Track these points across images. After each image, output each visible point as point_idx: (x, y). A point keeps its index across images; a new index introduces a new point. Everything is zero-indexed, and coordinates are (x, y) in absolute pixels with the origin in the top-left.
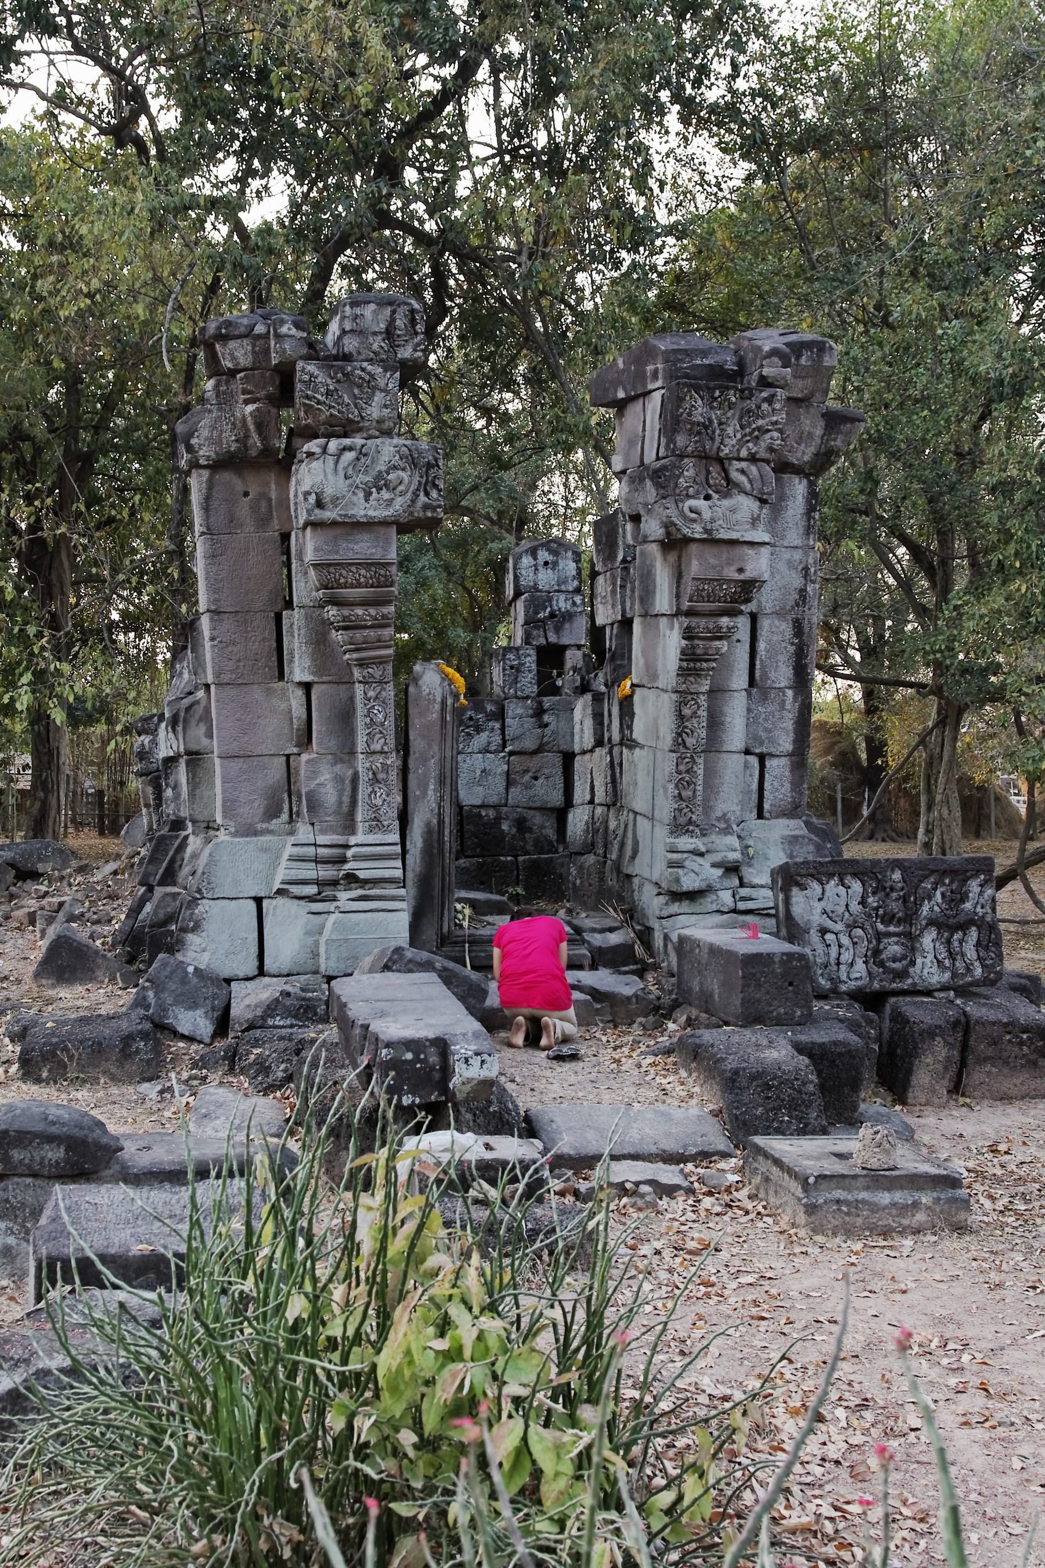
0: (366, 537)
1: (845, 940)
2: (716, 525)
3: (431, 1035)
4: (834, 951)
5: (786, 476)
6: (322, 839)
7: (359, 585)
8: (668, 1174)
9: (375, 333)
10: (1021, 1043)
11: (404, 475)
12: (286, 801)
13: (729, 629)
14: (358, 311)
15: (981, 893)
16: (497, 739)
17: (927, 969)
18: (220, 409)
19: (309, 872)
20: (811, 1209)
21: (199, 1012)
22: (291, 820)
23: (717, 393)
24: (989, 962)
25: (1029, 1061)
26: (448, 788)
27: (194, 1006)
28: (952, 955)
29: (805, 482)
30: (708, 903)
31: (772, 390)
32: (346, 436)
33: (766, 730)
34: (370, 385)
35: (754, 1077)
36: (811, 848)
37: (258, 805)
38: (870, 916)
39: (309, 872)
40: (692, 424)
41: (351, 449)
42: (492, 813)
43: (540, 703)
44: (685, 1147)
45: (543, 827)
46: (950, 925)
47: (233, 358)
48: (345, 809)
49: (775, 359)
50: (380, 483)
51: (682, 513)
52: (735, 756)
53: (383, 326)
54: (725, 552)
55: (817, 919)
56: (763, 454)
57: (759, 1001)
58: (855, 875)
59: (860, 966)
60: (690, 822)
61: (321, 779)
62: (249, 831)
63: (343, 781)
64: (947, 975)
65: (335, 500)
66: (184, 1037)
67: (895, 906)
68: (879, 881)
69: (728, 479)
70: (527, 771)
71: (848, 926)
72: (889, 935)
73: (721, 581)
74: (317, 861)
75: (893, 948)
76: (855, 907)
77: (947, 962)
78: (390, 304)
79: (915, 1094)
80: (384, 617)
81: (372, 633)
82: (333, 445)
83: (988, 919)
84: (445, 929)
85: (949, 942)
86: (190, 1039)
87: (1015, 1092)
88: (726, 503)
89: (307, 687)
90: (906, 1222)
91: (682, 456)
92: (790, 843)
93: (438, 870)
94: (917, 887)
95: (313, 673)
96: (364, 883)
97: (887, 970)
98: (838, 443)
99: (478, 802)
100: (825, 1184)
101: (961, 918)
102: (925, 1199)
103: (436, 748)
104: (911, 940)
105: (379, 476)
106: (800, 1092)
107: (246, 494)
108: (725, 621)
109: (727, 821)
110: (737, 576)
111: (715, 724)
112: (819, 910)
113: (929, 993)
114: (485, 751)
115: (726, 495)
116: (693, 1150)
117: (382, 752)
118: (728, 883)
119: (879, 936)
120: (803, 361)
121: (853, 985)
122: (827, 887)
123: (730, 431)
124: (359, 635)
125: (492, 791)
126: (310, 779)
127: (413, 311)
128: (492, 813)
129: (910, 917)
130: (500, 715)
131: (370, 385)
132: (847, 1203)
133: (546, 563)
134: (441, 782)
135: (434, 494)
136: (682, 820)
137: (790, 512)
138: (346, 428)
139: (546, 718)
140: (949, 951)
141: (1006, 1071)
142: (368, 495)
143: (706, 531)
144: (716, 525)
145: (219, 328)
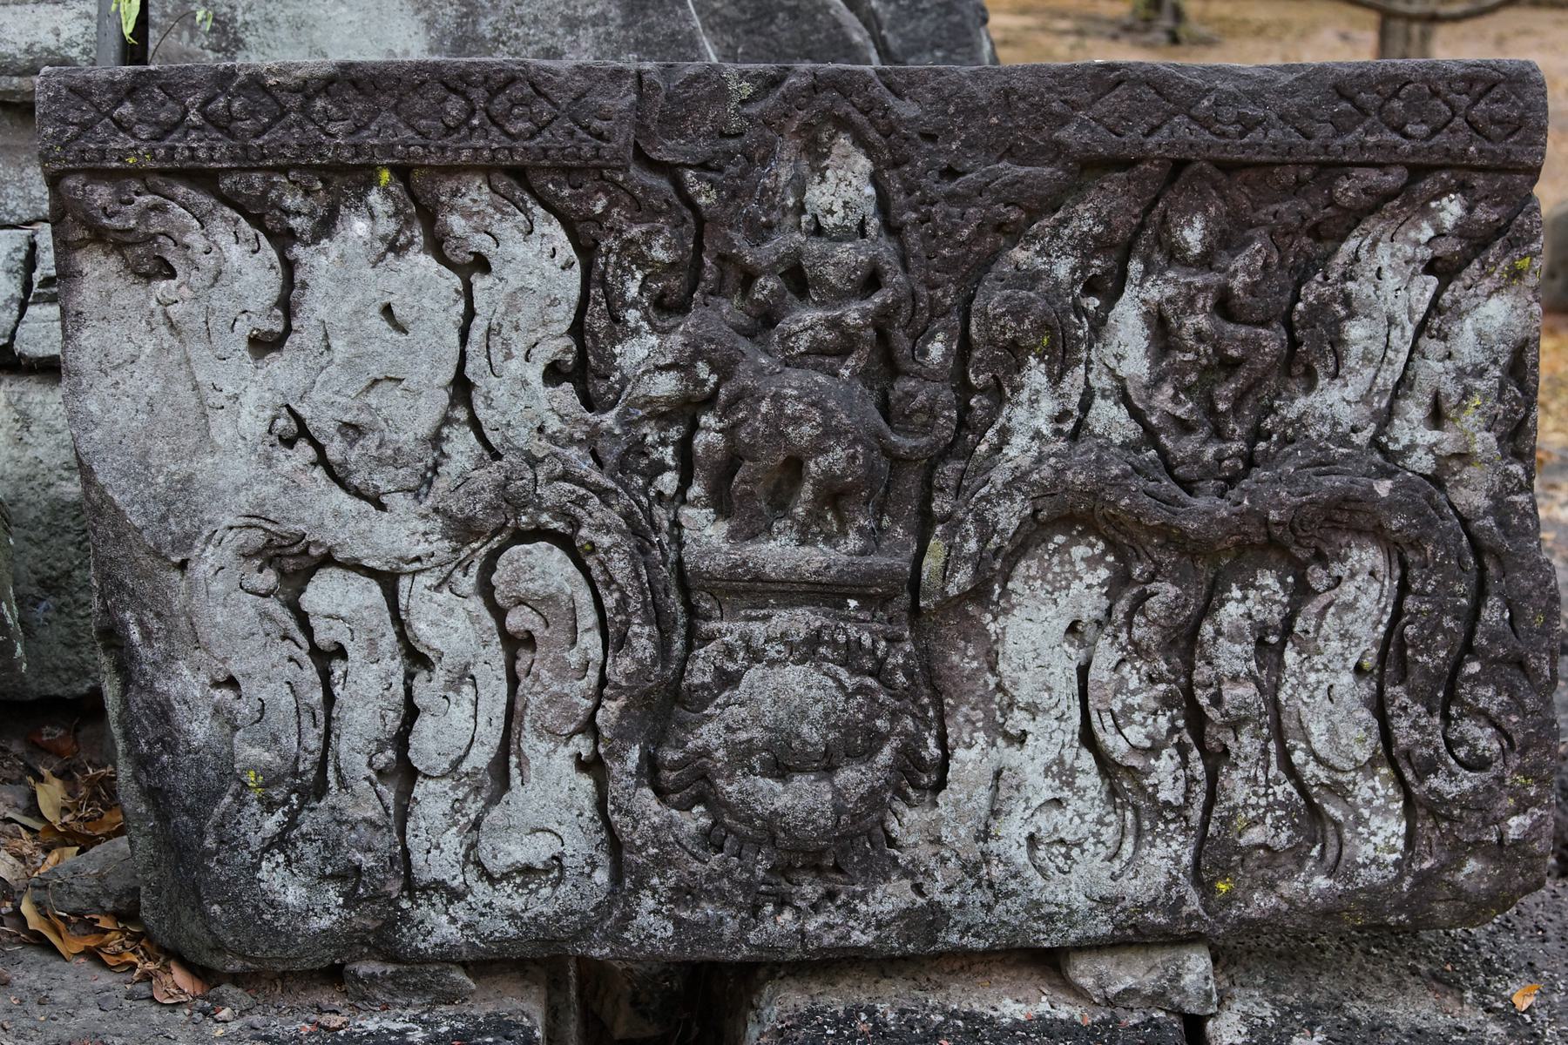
1: (449, 621)
15: (1434, 322)
28: (1194, 721)
46: (1198, 531)
55: (239, 474)
58: (520, 180)
59: (553, 786)
64: (1164, 858)
67: (804, 398)
72: (755, 590)
75: (782, 686)
76: (522, 400)
85: (1184, 641)
97: (731, 829)
101: (1276, 493)
104: (914, 651)
121: (502, 910)
129: (912, 473)
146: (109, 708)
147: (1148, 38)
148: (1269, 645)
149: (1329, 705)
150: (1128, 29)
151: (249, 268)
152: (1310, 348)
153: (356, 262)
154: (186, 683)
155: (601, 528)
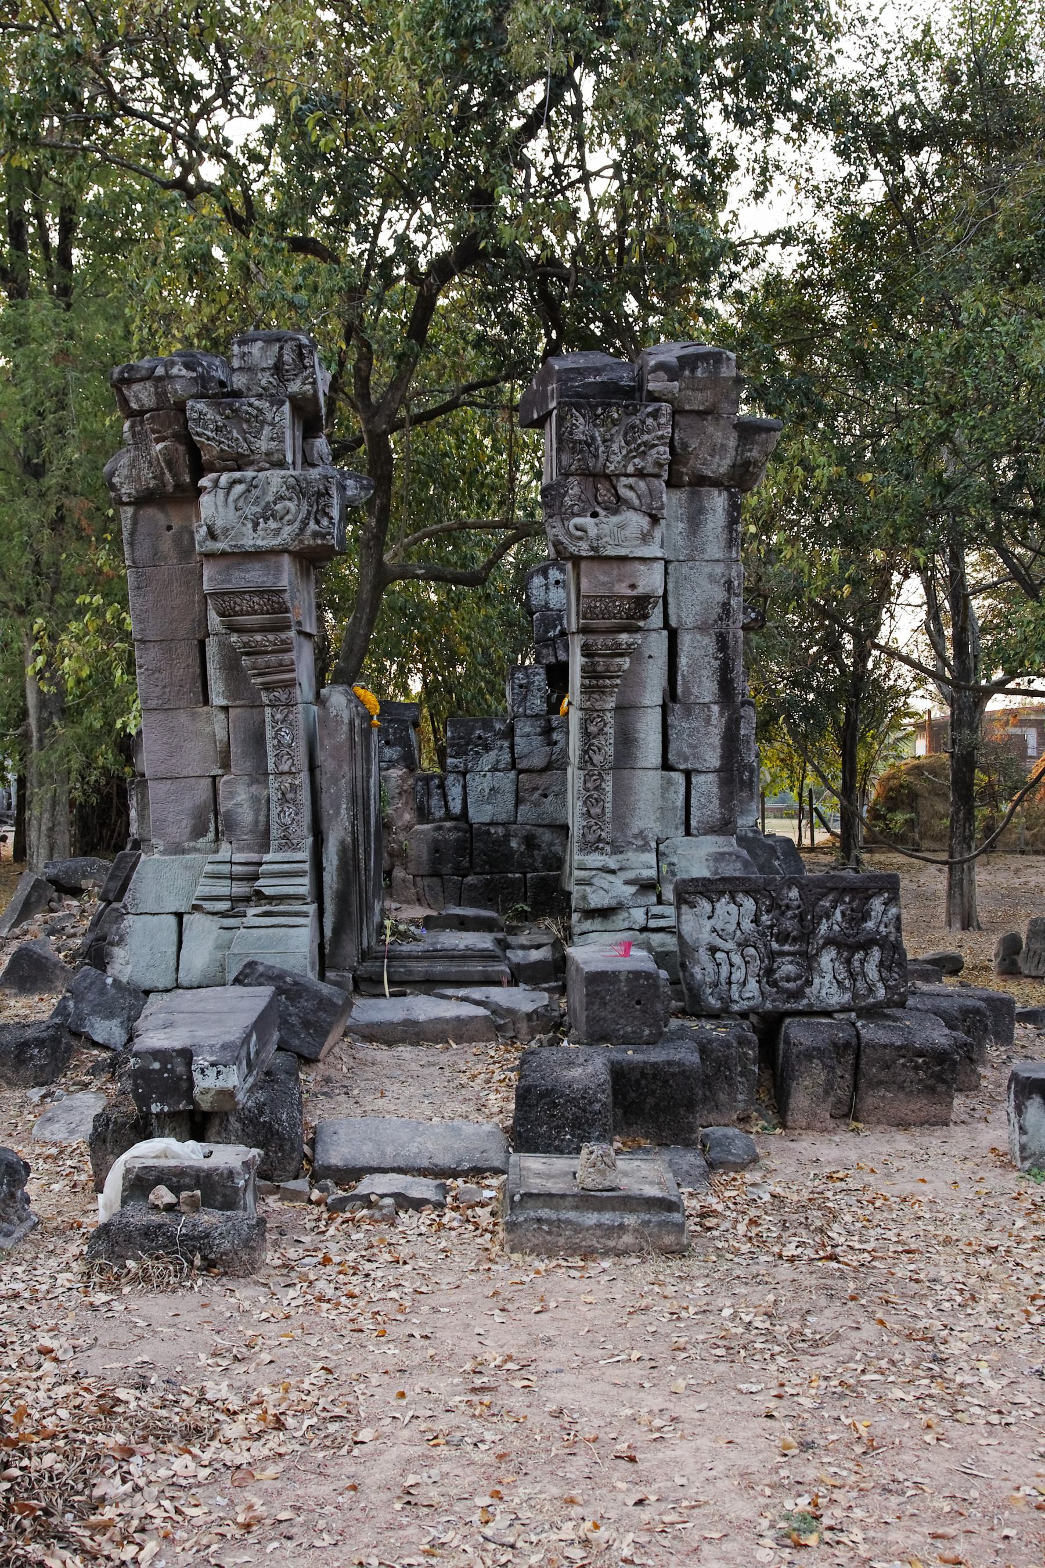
0: (257, 566)
1: (737, 959)
2: (601, 543)
3: (178, 1045)
4: (725, 970)
5: (704, 489)
6: (239, 857)
7: (255, 613)
8: (423, 1188)
9: (263, 370)
10: (917, 1068)
11: (292, 506)
12: (212, 821)
13: (629, 645)
15: (884, 912)
16: (506, 757)
17: (827, 987)
18: (137, 449)
19: (223, 888)
20: (511, 1227)
21: (116, 1022)
22: (217, 839)
23: (599, 411)
24: (892, 983)
25: (926, 1087)
26: (360, 807)
27: (110, 1016)
28: (852, 976)
29: (725, 494)
30: (620, 920)
31: (657, 405)
32: (239, 469)
33: (690, 746)
34: (259, 419)
35: (547, 1093)
36: (739, 865)
37: (186, 824)
38: (764, 935)
39: (223, 888)
40: (575, 442)
41: (240, 481)
42: (501, 831)
43: (549, 721)
44: (459, 1164)
45: (552, 844)
46: (851, 945)
47: (138, 400)
48: (261, 828)
49: (661, 374)
50: (268, 514)
51: (568, 532)
52: (651, 773)
53: (271, 362)
54: (615, 569)
55: (706, 937)
56: (650, 469)
57: (604, 1019)
58: (747, 893)
59: (753, 985)
60: (599, 839)
61: (238, 799)
62: (177, 850)
63: (259, 800)
64: (847, 996)
65: (226, 531)
66: (95, 1044)
67: (789, 925)
68: (773, 899)
69: (617, 496)
70: (536, 789)
71: (739, 945)
73: (613, 598)
74: (232, 878)
75: (787, 968)
76: (747, 926)
77: (847, 983)
78: (278, 340)
80: (283, 642)
81: (273, 658)
82: (225, 478)
83: (892, 938)
84: (365, 944)
85: (849, 962)
86: (105, 1047)
87: (912, 1117)
88: (614, 519)
89: (225, 709)
90: (611, 1243)
92: (716, 860)
93: (355, 888)
94: (815, 904)
95: (227, 698)
96: (271, 899)
97: (781, 990)
98: (755, 454)
99: (487, 819)
100: (531, 1203)
101: (861, 938)
102: (631, 1220)
103: (346, 768)
104: (808, 962)
106: (584, 1111)
107: (169, 528)
108: (624, 637)
109: (644, 838)
110: (630, 592)
111: (626, 741)
112: (708, 928)
113: (828, 1014)
114: (495, 769)
115: (615, 512)
116: (466, 1165)
117: (290, 773)
119: (773, 955)
120: (699, 373)
121: (745, 1005)
122: (718, 905)
123: (615, 447)
124: (261, 660)
125: (500, 808)
126: (227, 799)
127: (300, 346)
128: (501, 831)
129: (806, 935)
130: (509, 733)
131: (259, 419)
132: (549, 1222)
133: (557, 582)
134: (353, 799)
135: (325, 522)
136: (591, 838)
137: (710, 525)
138: (239, 462)
139: (555, 736)
140: (849, 971)
141: (901, 1096)
142: (256, 525)
143: (592, 548)
144: (601, 543)
145: (122, 372)
148: (862, 962)
152: (866, 916)
153: (723, 905)
154: (697, 970)
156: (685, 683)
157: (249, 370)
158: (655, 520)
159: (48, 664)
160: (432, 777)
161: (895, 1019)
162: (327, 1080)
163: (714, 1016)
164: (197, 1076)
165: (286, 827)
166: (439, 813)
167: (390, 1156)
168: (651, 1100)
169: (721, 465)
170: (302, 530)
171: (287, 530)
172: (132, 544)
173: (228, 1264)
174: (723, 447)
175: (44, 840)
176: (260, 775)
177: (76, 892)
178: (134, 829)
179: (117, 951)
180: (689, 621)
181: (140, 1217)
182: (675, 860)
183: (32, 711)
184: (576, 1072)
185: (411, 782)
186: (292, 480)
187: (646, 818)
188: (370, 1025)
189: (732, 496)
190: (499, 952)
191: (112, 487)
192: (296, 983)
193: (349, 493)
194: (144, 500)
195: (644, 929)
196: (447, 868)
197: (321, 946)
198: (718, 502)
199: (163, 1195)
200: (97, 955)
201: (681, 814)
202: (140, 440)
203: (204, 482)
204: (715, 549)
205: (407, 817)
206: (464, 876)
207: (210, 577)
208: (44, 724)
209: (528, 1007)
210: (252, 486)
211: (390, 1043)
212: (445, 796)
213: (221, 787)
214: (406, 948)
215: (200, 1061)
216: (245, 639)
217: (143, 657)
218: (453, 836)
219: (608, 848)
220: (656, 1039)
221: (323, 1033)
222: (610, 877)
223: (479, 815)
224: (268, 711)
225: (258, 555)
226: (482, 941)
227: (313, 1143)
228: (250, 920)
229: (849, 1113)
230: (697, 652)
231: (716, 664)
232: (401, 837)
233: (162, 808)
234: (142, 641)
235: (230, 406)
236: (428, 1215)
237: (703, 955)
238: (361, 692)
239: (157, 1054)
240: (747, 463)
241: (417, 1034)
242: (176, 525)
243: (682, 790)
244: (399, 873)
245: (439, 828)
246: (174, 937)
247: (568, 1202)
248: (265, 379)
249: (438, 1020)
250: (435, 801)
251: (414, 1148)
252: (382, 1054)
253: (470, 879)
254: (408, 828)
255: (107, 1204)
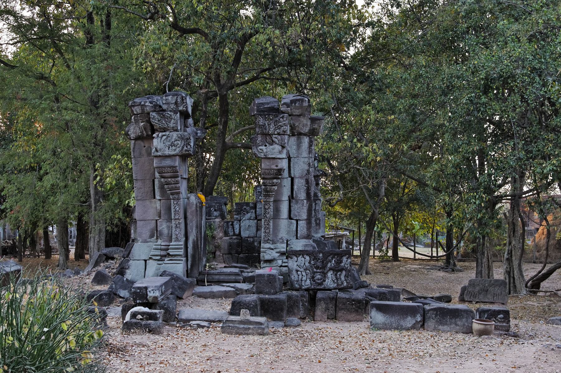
0: (169, 159)
1: (304, 274)
4: (300, 277)
6: (163, 244)
8: (205, 324)
10: (353, 305)
11: (179, 142)
12: (156, 233)
14: (167, 98)
15: (347, 261)
16: (254, 215)
17: (329, 282)
22: (157, 239)
25: (355, 310)
27: (125, 289)
28: (337, 279)
29: (308, 138)
30: (274, 264)
35: (239, 302)
38: (312, 267)
41: (165, 135)
42: (251, 240)
46: (337, 270)
47: (136, 111)
50: (172, 145)
53: (174, 101)
54: (272, 161)
55: (295, 267)
56: (282, 133)
58: (307, 255)
59: (308, 281)
60: (268, 240)
61: (163, 227)
62: (145, 241)
63: (169, 227)
64: (336, 285)
65: (160, 149)
66: (121, 297)
67: (319, 264)
69: (273, 141)
72: (317, 272)
73: (271, 169)
75: (318, 276)
76: (307, 264)
79: (317, 318)
80: (177, 181)
81: (174, 186)
82: (160, 134)
85: (336, 275)
86: (123, 298)
87: (352, 319)
88: (271, 147)
89: (160, 200)
91: (258, 134)
94: (327, 258)
96: (172, 256)
97: (316, 283)
98: (316, 126)
99: (247, 236)
100: (228, 322)
101: (340, 268)
102: (251, 327)
104: (324, 275)
105: (172, 143)
107: (145, 147)
108: (275, 181)
109: (283, 240)
111: (277, 211)
113: (330, 290)
114: (250, 219)
115: (272, 145)
117: (178, 219)
118: (281, 258)
119: (314, 273)
120: (297, 105)
121: (306, 287)
123: (271, 127)
124: (170, 186)
127: (182, 97)
128: (251, 240)
129: (324, 267)
132: (231, 327)
134: (197, 227)
135: (189, 147)
136: (266, 239)
138: (165, 130)
146: (254, 318)
147: (446, 270)
148: (340, 275)
149: (343, 278)
150: (443, 268)
151: (296, 258)
152: (341, 262)
153: (300, 258)
154: (292, 277)
155: (310, 270)
156: (296, 194)
157: (168, 104)
158: (283, 147)
159: (101, 179)
160: (229, 222)
161: (350, 292)
162: (185, 304)
163: (297, 290)
164: (148, 293)
165: (177, 235)
166: (231, 234)
167: (198, 317)
168: (271, 309)
169: (306, 130)
170: (182, 149)
171: (178, 149)
172: (134, 151)
173: (154, 331)
174: (307, 125)
175: (96, 246)
176: (170, 220)
177: (113, 259)
178: (132, 236)
179: (127, 271)
180: (297, 175)
181: (134, 320)
182: (292, 246)
183: (92, 196)
184: (248, 298)
185: (222, 223)
186: (179, 135)
187: (283, 234)
188: (200, 293)
189: (310, 138)
190: (240, 273)
191: (128, 135)
192: (177, 277)
193: (199, 135)
194: (137, 139)
195: (281, 266)
196: (233, 252)
197: (187, 271)
198: (306, 140)
199: (140, 317)
200: (121, 272)
201: (295, 232)
202: (136, 121)
203: (154, 135)
204: (305, 154)
205: (221, 234)
206: (239, 254)
207: (156, 163)
208: (97, 201)
209: (246, 288)
210: (168, 137)
211: (205, 298)
212: (233, 228)
213: (158, 223)
214: (212, 271)
215: (149, 289)
216: (166, 180)
217: (137, 185)
218: (235, 241)
219: (271, 242)
220: (275, 293)
221: (184, 291)
222: (271, 251)
223: (244, 234)
224: (172, 201)
225: (169, 156)
226: (236, 270)
227: (178, 315)
228: (166, 262)
229: (333, 318)
230: (299, 184)
231: (305, 188)
232: (219, 241)
233: (140, 230)
234: (136, 180)
235: (162, 114)
236: (206, 329)
237: (294, 272)
238: (199, 195)
239: (139, 288)
240: (314, 129)
241: (214, 296)
242: (147, 146)
243: (295, 226)
244: (218, 253)
245: (231, 238)
246: (144, 267)
247: (237, 322)
248: (172, 106)
249: (219, 291)
250: (230, 229)
251: (204, 316)
252: (204, 301)
253: (241, 255)
254: (221, 238)
255: (128, 318)
